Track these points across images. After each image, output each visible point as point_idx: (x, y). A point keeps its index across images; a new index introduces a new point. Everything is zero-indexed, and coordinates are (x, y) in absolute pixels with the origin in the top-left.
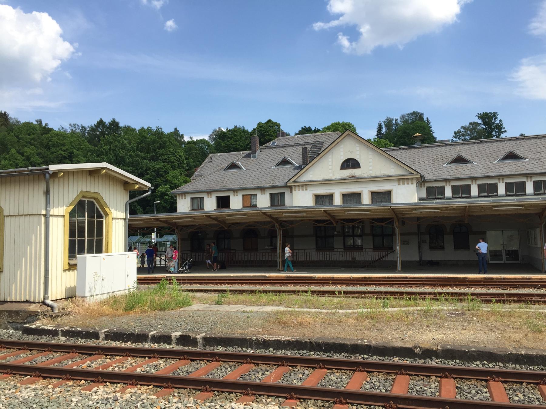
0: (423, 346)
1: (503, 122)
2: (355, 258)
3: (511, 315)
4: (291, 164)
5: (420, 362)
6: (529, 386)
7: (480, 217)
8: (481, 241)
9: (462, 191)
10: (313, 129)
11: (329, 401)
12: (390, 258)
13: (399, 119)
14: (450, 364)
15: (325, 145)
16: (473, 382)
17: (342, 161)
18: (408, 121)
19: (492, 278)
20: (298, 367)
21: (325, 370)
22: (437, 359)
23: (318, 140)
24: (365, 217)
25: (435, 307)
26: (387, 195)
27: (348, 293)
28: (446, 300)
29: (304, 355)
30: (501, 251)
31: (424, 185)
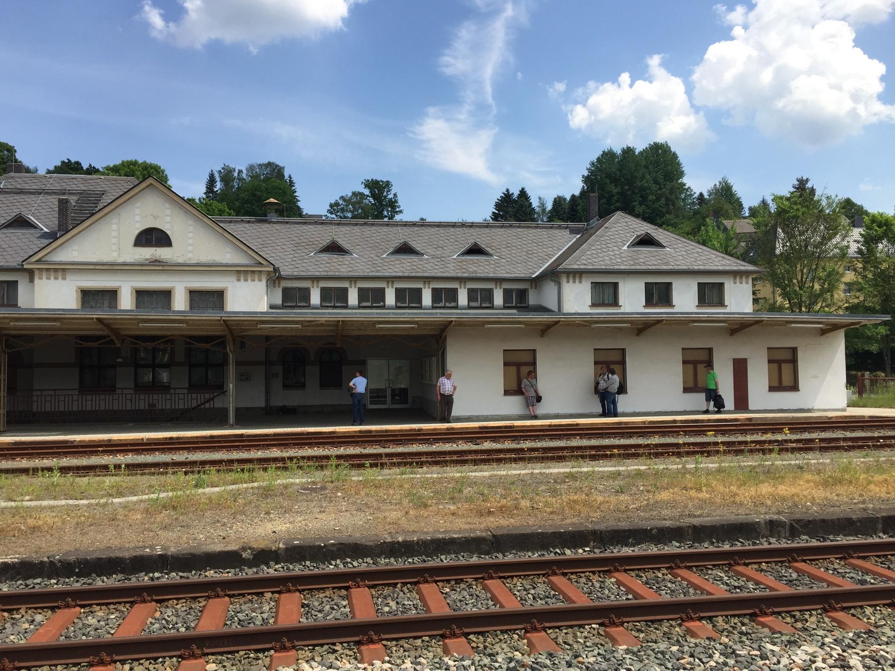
0: (255, 546)
1: (399, 198)
2: (153, 405)
3: (389, 484)
4: (34, 227)
5: (249, 573)
6: (405, 589)
7: (358, 338)
8: (358, 374)
9: (335, 297)
10: (85, 166)
11: (79, 664)
12: (218, 403)
13: (245, 171)
14: (297, 569)
15: (106, 199)
16: (328, 593)
17: (137, 232)
18: (259, 176)
19: (370, 431)
20: (22, 611)
21: (78, 609)
22: (277, 564)
23: (91, 188)
24: (176, 333)
25: (282, 480)
26: (218, 296)
27: (132, 468)
28: (300, 468)
29: (37, 586)
30: (385, 390)
31: (279, 283)
